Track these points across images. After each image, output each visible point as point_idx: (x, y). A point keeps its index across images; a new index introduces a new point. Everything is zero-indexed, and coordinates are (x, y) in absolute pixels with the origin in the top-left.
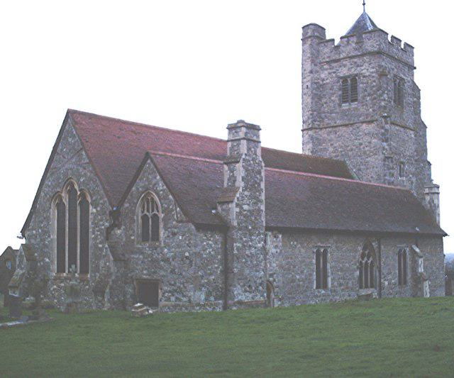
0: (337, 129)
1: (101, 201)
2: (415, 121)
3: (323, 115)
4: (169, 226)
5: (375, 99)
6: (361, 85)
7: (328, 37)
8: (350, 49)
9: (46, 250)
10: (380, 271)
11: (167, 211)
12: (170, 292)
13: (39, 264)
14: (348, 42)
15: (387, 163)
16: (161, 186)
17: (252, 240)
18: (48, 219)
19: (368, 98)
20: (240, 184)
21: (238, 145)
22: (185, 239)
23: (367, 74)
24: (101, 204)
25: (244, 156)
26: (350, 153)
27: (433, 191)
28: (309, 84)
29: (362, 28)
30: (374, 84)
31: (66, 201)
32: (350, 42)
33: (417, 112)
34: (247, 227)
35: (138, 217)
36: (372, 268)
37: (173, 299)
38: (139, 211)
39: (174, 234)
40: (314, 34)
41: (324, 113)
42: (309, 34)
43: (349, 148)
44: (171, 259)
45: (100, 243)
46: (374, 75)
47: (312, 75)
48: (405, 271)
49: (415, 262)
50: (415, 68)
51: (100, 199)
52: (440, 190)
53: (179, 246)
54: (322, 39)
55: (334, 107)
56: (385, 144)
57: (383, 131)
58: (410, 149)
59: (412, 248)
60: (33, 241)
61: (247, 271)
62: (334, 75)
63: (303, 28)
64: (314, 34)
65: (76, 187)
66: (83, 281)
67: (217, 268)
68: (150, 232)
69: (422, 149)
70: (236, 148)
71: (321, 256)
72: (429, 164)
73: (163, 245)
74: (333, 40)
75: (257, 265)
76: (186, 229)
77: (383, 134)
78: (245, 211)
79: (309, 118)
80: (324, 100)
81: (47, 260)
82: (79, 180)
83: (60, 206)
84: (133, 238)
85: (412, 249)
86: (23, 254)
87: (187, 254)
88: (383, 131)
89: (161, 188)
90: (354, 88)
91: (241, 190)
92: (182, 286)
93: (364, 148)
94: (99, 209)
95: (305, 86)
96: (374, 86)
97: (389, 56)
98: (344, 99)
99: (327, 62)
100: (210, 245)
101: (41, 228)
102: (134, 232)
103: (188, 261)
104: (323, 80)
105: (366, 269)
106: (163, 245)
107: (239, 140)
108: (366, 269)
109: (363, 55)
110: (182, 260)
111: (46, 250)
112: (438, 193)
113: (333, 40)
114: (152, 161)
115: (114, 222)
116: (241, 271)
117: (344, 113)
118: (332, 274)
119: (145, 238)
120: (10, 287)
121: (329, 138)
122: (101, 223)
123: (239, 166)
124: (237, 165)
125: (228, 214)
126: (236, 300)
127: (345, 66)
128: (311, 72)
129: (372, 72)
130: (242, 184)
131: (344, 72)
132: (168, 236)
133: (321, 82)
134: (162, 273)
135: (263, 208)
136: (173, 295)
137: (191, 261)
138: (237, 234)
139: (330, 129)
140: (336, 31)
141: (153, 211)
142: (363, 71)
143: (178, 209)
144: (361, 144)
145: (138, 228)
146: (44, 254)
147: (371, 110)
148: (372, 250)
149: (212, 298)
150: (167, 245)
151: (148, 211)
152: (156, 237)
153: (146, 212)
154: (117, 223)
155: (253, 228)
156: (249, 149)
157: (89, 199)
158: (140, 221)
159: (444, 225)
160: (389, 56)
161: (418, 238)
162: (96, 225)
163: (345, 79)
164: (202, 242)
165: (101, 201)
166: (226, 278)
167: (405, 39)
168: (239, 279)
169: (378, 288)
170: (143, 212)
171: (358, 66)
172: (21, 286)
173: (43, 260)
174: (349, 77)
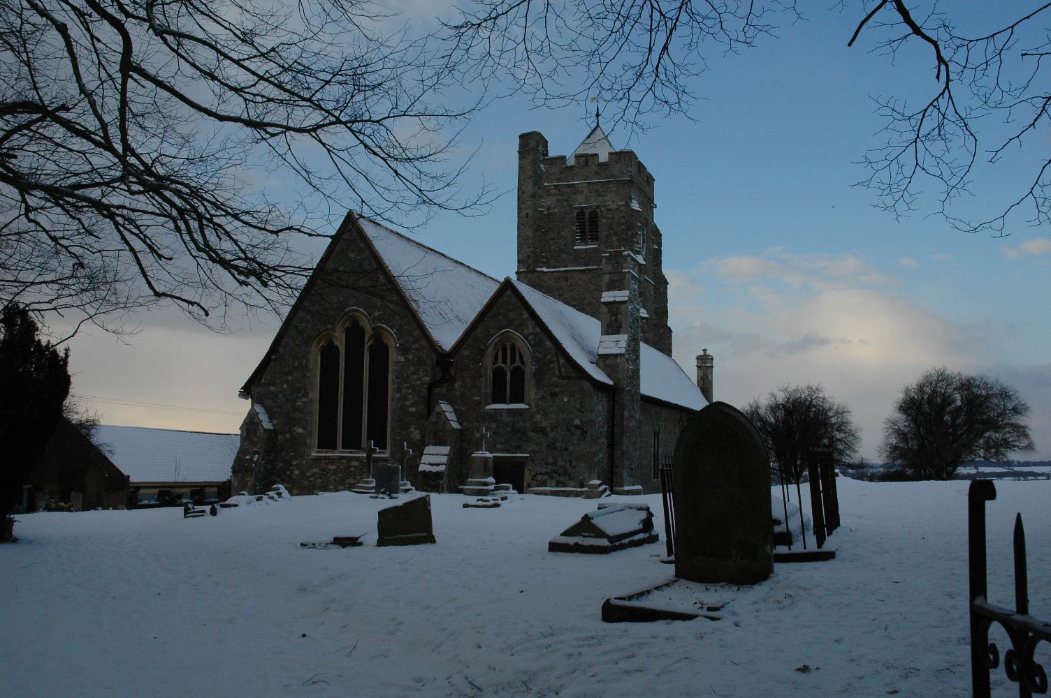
2: (655, 274)
6: (604, 221)
7: (553, 152)
9: (297, 415)
12: (546, 473)
13: (281, 437)
19: (614, 238)
30: (623, 221)
31: (340, 341)
32: (590, 163)
39: (554, 395)
43: (586, 301)
45: (412, 405)
51: (414, 343)
55: (565, 245)
62: (565, 203)
63: (522, 137)
64: (532, 145)
65: (365, 323)
67: (603, 443)
72: (670, 331)
74: (563, 158)
79: (528, 257)
80: (550, 236)
81: (300, 430)
83: (329, 353)
87: (577, 422)
89: (531, 331)
92: (568, 465)
94: (411, 357)
95: (523, 213)
96: (622, 224)
101: (287, 382)
103: (579, 432)
110: (569, 430)
111: (297, 415)
112: (712, 367)
128: (533, 196)
129: (621, 206)
131: (580, 202)
132: (543, 397)
141: (513, 361)
142: (608, 203)
143: (562, 361)
151: (504, 361)
153: (500, 364)
154: (447, 377)
159: (126, 473)
170: (494, 363)
171: (600, 195)
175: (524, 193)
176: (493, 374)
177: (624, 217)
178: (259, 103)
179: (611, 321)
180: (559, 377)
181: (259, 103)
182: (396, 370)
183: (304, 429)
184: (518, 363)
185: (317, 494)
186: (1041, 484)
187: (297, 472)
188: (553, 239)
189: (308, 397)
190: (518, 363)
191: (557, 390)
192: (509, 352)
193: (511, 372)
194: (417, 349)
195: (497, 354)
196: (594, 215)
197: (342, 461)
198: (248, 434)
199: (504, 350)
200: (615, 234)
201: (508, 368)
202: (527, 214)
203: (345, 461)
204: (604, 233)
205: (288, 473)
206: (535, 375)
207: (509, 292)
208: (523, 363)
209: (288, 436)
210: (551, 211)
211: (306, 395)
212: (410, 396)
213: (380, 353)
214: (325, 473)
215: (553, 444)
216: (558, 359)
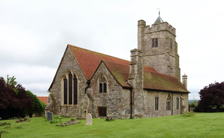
0: (150, 56)
1: (83, 78)
3: (145, 51)
4: (111, 87)
5: (164, 46)
7: (147, 25)
8: (155, 29)
9: (59, 96)
10: (172, 104)
11: (110, 82)
13: (56, 101)
14: (155, 26)
15: (168, 68)
16: (108, 72)
17: (139, 93)
18: (60, 85)
20: (136, 72)
21: (135, 58)
22: (118, 92)
23: (162, 38)
24: (83, 79)
25: (137, 62)
26: (155, 65)
27: (185, 78)
28: (141, 41)
29: (158, 22)
30: (164, 41)
31: (67, 77)
33: (176, 51)
34: (138, 88)
35: (98, 84)
36: (170, 103)
37: (113, 114)
38: (98, 82)
39: (113, 90)
40: (142, 24)
41: (146, 51)
42: (140, 24)
46: (164, 38)
47: (141, 38)
48: (178, 104)
49: (181, 101)
50: (176, 37)
51: (82, 77)
52: (188, 77)
53: (115, 95)
54: (145, 26)
56: (168, 62)
57: (167, 57)
58: (174, 64)
59: (180, 96)
60: (54, 93)
61: (138, 104)
62: (149, 38)
63: (138, 21)
64: (142, 24)
65: (72, 73)
66: (75, 107)
67: (128, 103)
68: (103, 89)
69: (178, 64)
70: (134, 59)
71: (157, 99)
72: (180, 69)
73: (108, 94)
74: (149, 26)
75: (140, 102)
76: (118, 89)
77: (167, 58)
78: (138, 82)
80: (146, 46)
81: (60, 100)
82: (73, 70)
83: (65, 80)
84: (96, 91)
85: (180, 97)
86: (50, 98)
88: (167, 57)
89: (108, 73)
90: (157, 42)
91: (137, 75)
92: (116, 109)
93: (160, 63)
94: (82, 81)
95: (139, 41)
96: (164, 42)
97: (169, 32)
98: (153, 46)
99: (147, 34)
100: (126, 94)
102: (96, 89)
103: (119, 100)
104: (145, 40)
105: (71, 98)
106: (108, 94)
107: (136, 56)
108: (71, 98)
109: (160, 31)
111: (59, 96)
113: (149, 26)
114: (104, 63)
115: (88, 86)
116: (136, 104)
117: (153, 51)
118: (160, 105)
119: (101, 91)
120: (45, 110)
121: (148, 59)
122: (82, 86)
123: (136, 66)
124: (135, 65)
125: (132, 83)
126: (135, 114)
127: (153, 35)
129: (164, 37)
130: (137, 72)
131: (153, 37)
134: (108, 104)
135: (143, 81)
137: (120, 100)
138: (135, 91)
139: (148, 56)
140: (150, 22)
141: (104, 82)
143: (115, 81)
144: (159, 62)
145: (98, 88)
146: (58, 98)
147: (163, 50)
148: (170, 97)
149: (127, 114)
150: (110, 94)
151: (102, 82)
152: (105, 91)
153: (101, 82)
155: (140, 88)
156: (139, 59)
157: (77, 77)
158: (99, 85)
160: (169, 32)
161: (182, 93)
162: (80, 87)
163: (153, 39)
164: (124, 93)
165: (83, 78)
166: (131, 106)
167: (173, 26)
168: (136, 107)
169: (171, 110)
170: (100, 82)
172: (50, 109)
173: (58, 100)
174: (155, 38)
175: (139, 36)
176: (100, 85)
177: (164, 40)
178: (153, 32)
179: (132, 69)
180: (114, 86)
181: (153, 32)
184: (105, 82)
185: (185, 77)
190: (105, 82)
191: (114, 89)
192: (103, 79)
193: (104, 85)
195: (100, 79)
196: (157, 39)
199: (102, 79)
200: (162, 45)
201: (103, 83)
206: (109, 85)
207: (103, 63)
208: (106, 82)
210: (146, 40)
211: (61, 91)
212: (82, 91)
215: (113, 103)
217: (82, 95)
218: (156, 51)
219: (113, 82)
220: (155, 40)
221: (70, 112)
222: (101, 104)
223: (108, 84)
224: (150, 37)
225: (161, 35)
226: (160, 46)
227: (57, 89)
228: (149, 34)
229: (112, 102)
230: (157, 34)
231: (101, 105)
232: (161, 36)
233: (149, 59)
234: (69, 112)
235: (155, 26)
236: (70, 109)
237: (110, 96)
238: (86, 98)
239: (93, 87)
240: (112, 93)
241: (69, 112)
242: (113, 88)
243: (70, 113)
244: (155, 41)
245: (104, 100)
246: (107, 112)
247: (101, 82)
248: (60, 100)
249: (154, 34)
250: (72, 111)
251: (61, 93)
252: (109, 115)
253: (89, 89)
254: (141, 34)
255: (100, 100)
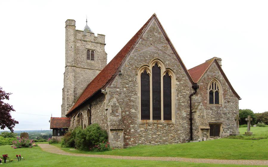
3: (78, 62)
5: (102, 62)
9: (132, 103)
11: (225, 91)
14: (91, 35)
31: (150, 72)
37: (229, 132)
41: (78, 61)
44: (227, 114)
62: (83, 46)
76: (234, 100)
80: (78, 56)
81: (133, 111)
87: (235, 111)
89: (222, 79)
90: (93, 55)
94: (182, 82)
96: (102, 57)
102: (207, 98)
104: (78, 47)
105: (157, 110)
106: (223, 106)
108: (157, 110)
109: (97, 43)
111: (132, 103)
117: (88, 64)
119: (211, 102)
122: (183, 91)
127: (89, 45)
129: (102, 51)
131: (89, 47)
133: (77, 48)
134: (222, 120)
136: (228, 130)
141: (215, 89)
143: (230, 90)
150: (225, 107)
151: (213, 89)
152: (217, 102)
153: (211, 89)
165: (184, 79)
170: (210, 89)
174: (91, 49)
180: (230, 96)
182: (176, 87)
183: (136, 110)
186: (267, 127)
187: (133, 130)
188: (79, 57)
189: (137, 95)
194: (184, 80)
196: (93, 51)
197: (155, 125)
198: (112, 111)
200: (100, 60)
201: (214, 91)
202: (71, 47)
203: (156, 125)
204: (96, 59)
205: (128, 130)
209: (127, 113)
212: (182, 99)
213: (168, 79)
214: (147, 130)
216: (229, 90)
217: (183, 105)
218: (93, 64)
219: (228, 92)
220: (90, 52)
221: (159, 133)
222: (213, 119)
223: (221, 92)
224: (84, 46)
225: (98, 48)
226: (98, 60)
227: (125, 89)
228: (83, 42)
229: (228, 117)
230: (94, 45)
231: (213, 121)
232: (98, 50)
233: (83, 72)
234: (157, 133)
235: (91, 35)
236: (159, 128)
237: (225, 109)
238: (201, 109)
239: (201, 94)
240: (228, 105)
241: (157, 133)
242: (228, 99)
243: (159, 135)
244: (90, 52)
245: (217, 113)
246: (221, 129)
247: (211, 89)
248: (133, 111)
249: (90, 43)
250: (162, 132)
251: (136, 98)
252: (224, 134)
253: (194, 97)
254: (73, 37)
255: (212, 114)
